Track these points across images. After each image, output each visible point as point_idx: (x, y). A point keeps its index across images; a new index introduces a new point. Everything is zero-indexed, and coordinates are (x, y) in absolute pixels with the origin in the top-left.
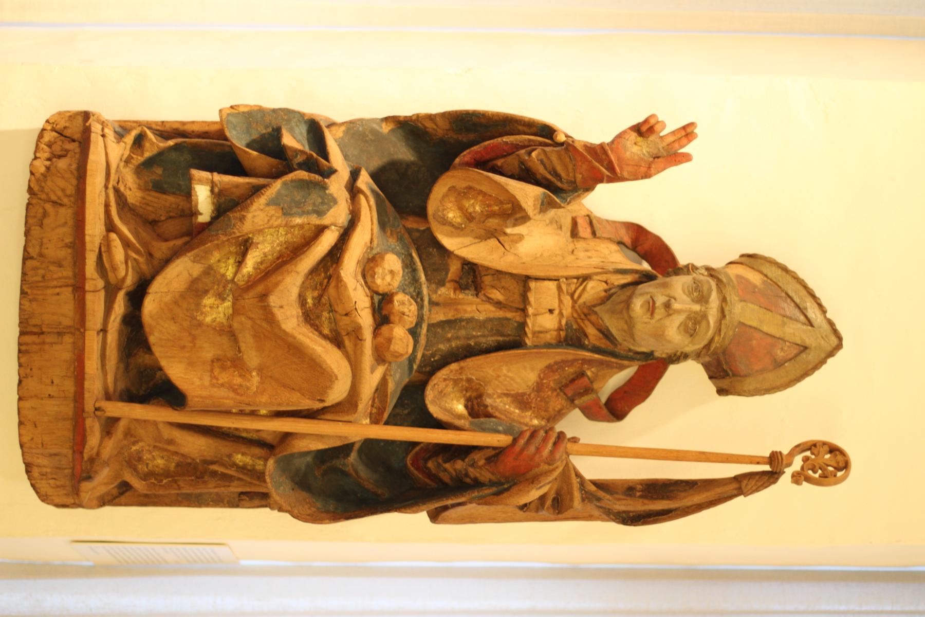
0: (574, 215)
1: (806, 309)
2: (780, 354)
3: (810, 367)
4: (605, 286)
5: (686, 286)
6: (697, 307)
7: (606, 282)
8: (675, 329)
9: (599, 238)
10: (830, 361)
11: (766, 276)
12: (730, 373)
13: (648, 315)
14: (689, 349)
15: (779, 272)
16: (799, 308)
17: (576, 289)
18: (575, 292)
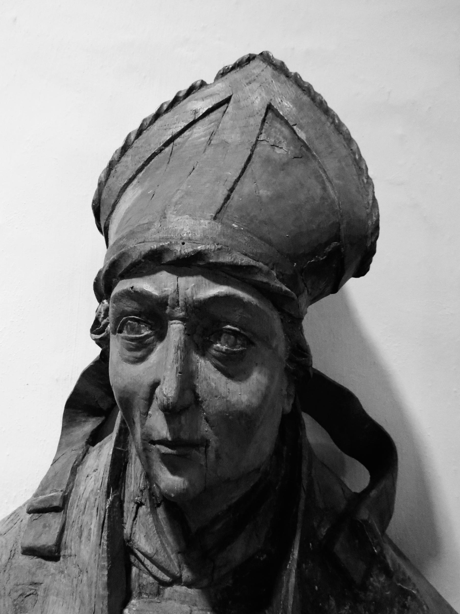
0: (20, 550)
1: (196, 112)
2: (283, 152)
3: (305, 98)
4: (143, 510)
5: (128, 354)
6: (176, 329)
7: (139, 505)
8: (233, 386)
9: (65, 499)
10: (292, 69)
11: (131, 181)
12: (334, 244)
13: (198, 454)
14: (280, 344)
15: (126, 159)
16: (194, 122)
17: (150, 573)
18: (155, 577)
